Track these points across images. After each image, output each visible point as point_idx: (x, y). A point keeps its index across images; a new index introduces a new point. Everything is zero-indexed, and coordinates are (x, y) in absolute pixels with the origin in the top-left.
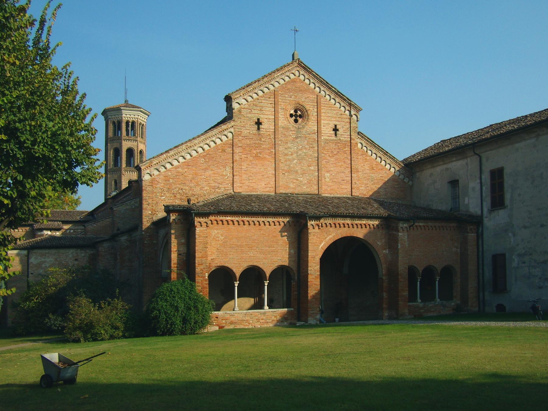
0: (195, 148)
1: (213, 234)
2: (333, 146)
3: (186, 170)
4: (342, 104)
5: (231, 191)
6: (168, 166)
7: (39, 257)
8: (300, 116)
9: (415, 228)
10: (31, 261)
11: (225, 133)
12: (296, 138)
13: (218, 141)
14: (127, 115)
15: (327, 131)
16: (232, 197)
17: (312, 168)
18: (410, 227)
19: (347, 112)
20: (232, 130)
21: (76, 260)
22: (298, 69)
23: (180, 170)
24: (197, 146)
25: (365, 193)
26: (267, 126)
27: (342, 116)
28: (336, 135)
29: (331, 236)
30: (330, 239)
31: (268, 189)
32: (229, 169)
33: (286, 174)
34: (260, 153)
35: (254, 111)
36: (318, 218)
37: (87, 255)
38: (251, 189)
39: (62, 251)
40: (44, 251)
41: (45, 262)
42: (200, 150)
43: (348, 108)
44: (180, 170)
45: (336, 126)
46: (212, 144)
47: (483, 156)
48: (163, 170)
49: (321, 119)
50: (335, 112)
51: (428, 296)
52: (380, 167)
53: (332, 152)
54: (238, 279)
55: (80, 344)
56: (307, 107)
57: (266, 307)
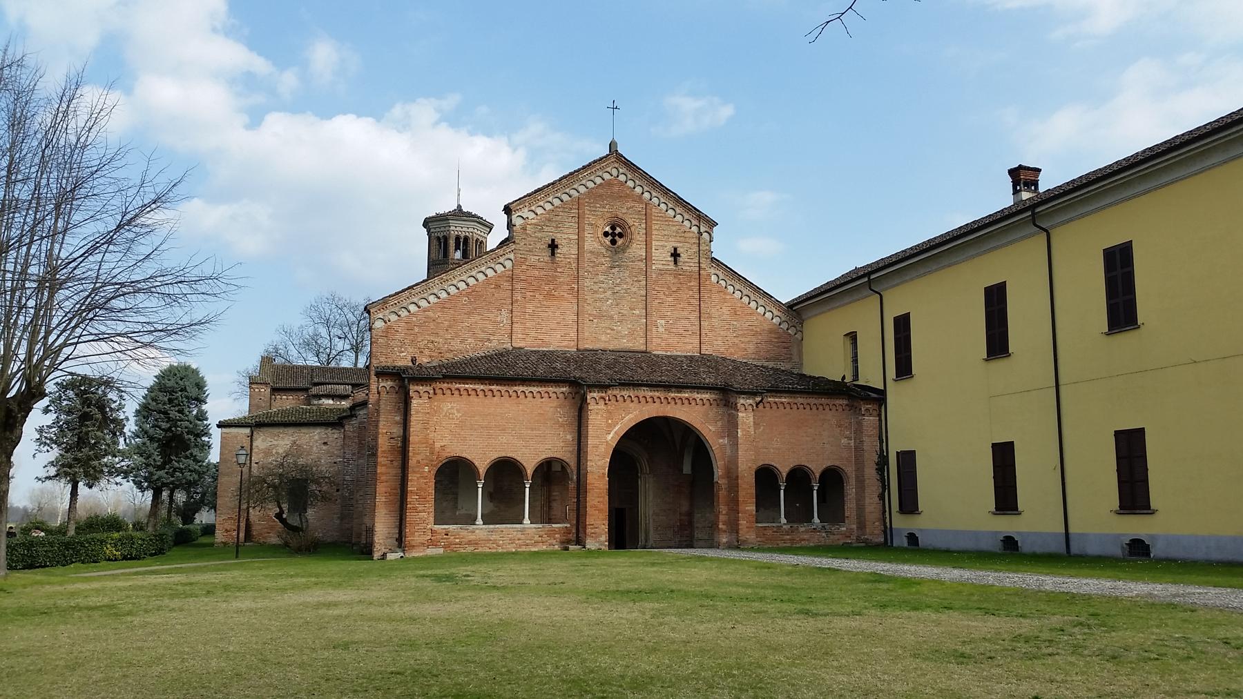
0: (455, 282)
2: (670, 279)
4: (686, 216)
5: (509, 346)
6: (413, 308)
8: (621, 235)
9: (767, 405)
11: (501, 260)
12: (612, 268)
13: (490, 273)
14: (457, 228)
15: (661, 256)
16: (499, 356)
18: (757, 404)
19: (695, 229)
20: (512, 256)
21: (325, 443)
23: (430, 314)
25: (722, 350)
26: (567, 250)
28: (676, 262)
29: (631, 416)
30: (630, 420)
31: (565, 343)
32: (504, 316)
35: (546, 229)
36: (603, 387)
39: (304, 430)
40: (276, 431)
42: (462, 286)
43: (695, 222)
44: (430, 314)
45: (675, 249)
46: (481, 277)
48: (404, 313)
51: (799, 514)
53: (669, 288)
54: (482, 476)
55: (364, 565)
56: (630, 222)
57: (527, 521)
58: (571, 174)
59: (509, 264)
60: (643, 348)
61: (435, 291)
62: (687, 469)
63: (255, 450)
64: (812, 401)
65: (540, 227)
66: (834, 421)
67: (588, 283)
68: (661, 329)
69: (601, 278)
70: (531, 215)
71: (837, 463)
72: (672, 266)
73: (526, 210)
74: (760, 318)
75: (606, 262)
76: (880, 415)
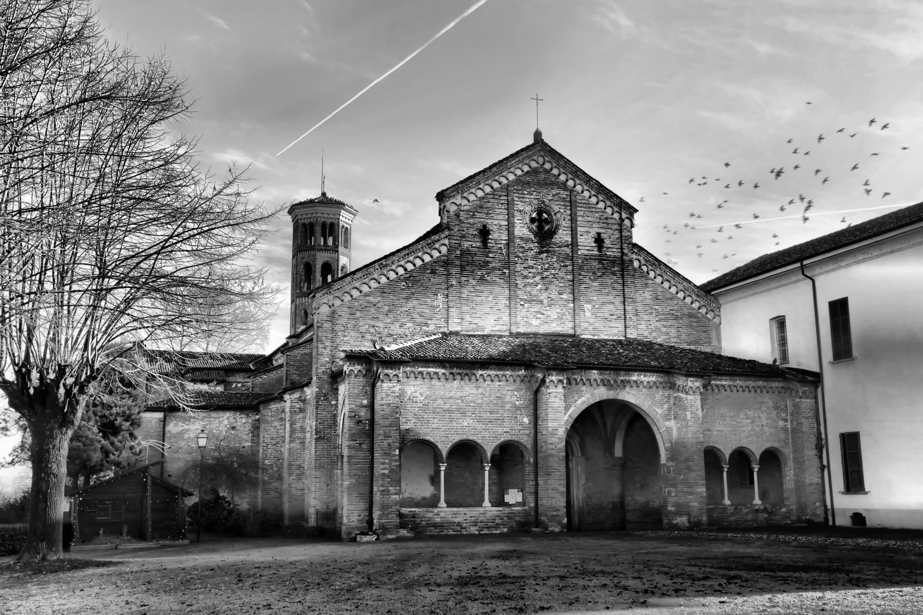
0: (394, 267)
1: (409, 393)
3: (379, 299)
6: (355, 293)
7: (180, 424)
10: (167, 429)
11: (437, 246)
12: (540, 253)
14: (324, 215)
17: (565, 296)
19: (616, 216)
22: (542, 154)
23: (371, 299)
24: (396, 265)
25: (646, 334)
27: (610, 221)
29: (583, 399)
31: (497, 328)
33: (526, 305)
34: (488, 274)
35: (478, 215)
37: (250, 421)
38: (474, 326)
41: (189, 430)
43: (616, 209)
44: (371, 299)
47: (818, 281)
49: (576, 225)
50: (597, 215)
52: (668, 296)
58: (500, 162)
59: (444, 250)
60: (571, 332)
61: (376, 276)
62: (618, 452)
63: (167, 435)
64: (751, 383)
65: (472, 213)
66: (770, 404)
67: (519, 268)
68: (588, 314)
69: (531, 263)
70: (465, 202)
71: (776, 445)
72: (596, 252)
73: (459, 197)
74: (680, 303)
75: (535, 247)
76: (816, 398)
